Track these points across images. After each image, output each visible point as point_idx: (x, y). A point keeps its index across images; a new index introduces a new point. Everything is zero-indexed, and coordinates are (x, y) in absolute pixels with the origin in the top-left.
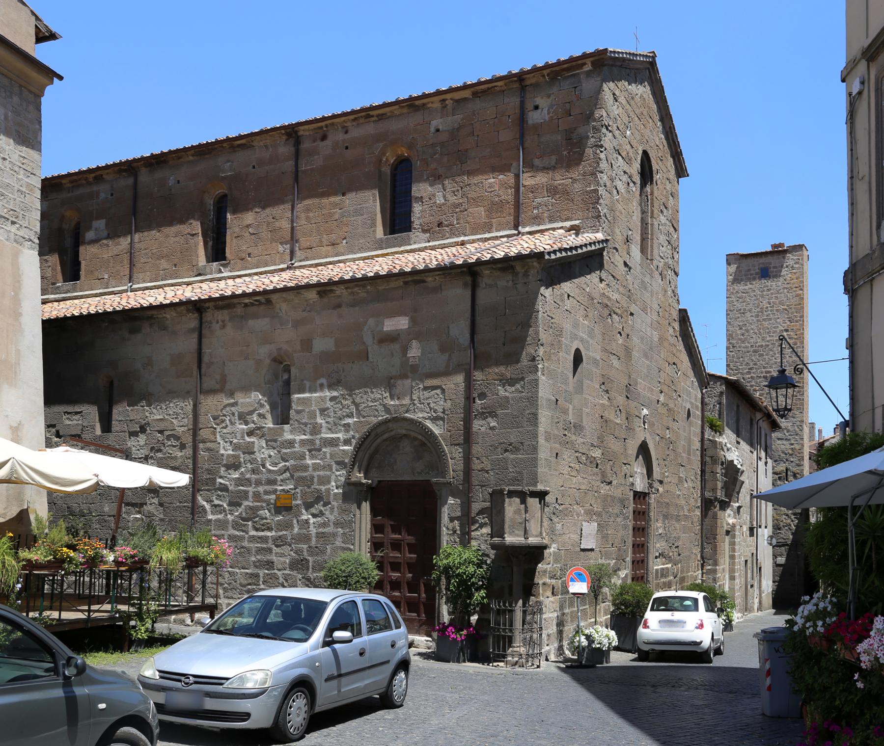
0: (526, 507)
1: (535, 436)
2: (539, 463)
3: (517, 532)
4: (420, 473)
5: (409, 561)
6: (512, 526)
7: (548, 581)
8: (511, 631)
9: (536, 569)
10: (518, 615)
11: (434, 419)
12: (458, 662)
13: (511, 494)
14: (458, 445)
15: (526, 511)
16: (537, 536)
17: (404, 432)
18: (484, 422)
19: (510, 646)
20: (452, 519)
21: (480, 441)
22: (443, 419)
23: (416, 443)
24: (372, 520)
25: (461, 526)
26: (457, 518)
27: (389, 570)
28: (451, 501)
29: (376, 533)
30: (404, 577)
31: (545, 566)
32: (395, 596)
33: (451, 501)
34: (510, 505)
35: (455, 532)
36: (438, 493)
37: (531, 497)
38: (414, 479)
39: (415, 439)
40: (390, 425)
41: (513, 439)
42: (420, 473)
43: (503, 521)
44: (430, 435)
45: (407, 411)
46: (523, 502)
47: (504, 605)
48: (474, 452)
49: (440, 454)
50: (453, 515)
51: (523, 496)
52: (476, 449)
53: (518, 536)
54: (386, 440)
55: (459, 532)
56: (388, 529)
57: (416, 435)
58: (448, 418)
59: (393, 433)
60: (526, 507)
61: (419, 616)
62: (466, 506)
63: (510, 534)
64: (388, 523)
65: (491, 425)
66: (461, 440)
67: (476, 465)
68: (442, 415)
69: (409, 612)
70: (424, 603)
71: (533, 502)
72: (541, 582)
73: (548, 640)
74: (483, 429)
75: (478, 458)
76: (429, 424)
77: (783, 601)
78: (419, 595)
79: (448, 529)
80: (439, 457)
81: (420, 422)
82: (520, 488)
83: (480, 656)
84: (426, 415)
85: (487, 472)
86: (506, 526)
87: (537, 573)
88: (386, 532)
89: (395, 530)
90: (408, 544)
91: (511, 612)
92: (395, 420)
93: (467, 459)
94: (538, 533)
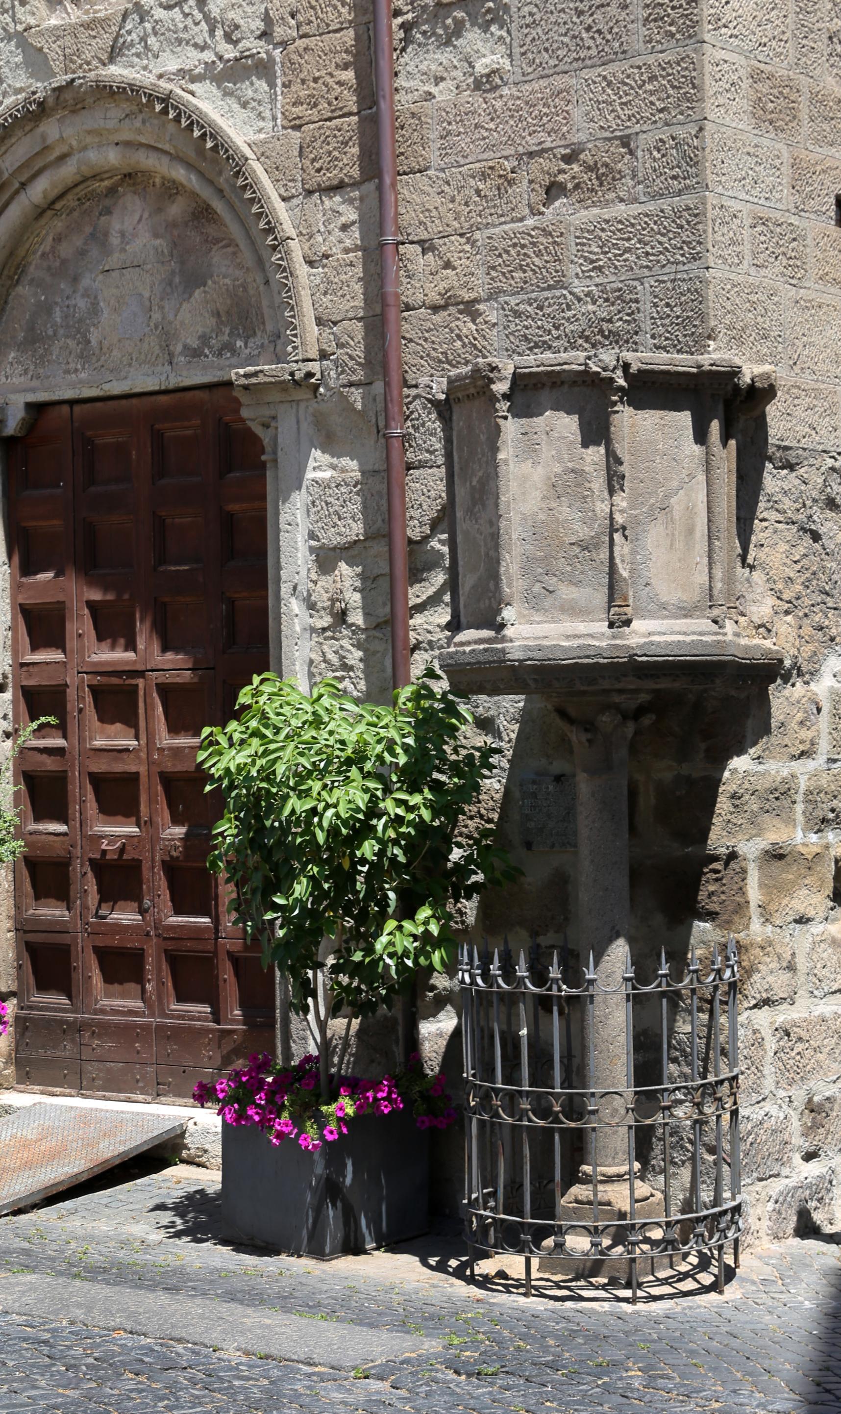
0: (613, 459)
1: (685, 90)
2: (715, 236)
3: (567, 592)
4: (195, 353)
5: (170, 766)
6: (542, 567)
7: (800, 838)
8: (575, 1108)
9: (715, 783)
10: (612, 1023)
11: (231, 74)
12: (318, 1253)
13: (532, 392)
14: (338, 187)
15: (614, 481)
16: (686, 612)
17: (112, 157)
18: (446, 56)
19: (572, 1177)
20: (326, 559)
21: (434, 157)
22: (263, 69)
23: (176, 209)
24: (16, 588)
25: (369, 584)
26: (347, 551)
27: (92, 806)
28: (320, 467)
29: (35, 647)
30: (154, 839)
31: (777, 768)
32: (118, 928)
33: (320, 467)
34: (530, 448)
35: (341, 617)
36: (265, 436)
37: (638, 404)
38: (175, 381)
39: (172, 189)
40: (50, 129)
41: (582, 126)
42: (195, 353)
43: (495, 538)
44: (211, 153)
45: (114, 54)
46: (596, 431)
47: (540, 977)
48: (408, 216)
49: (264, 239)
50: (331, 537)
51: (590, 399)
52: (418, 201)
53: (573, 610)
54: (42, 212)
55: (357, 618)
56: (80, 625)
57: (180, 173)
58: (292, 66)
59: (68, 171)
60: (613, 459)
61: (216, 1017)
62: (381, 492)
63: (533, 602)
64: (78, 595)
65: (481, 67)
66: (348, 163)
67: (419, 279)
68: (259, 48)
69: (180, 999)
70: (234, 959)
71: (657, 435)
72: (750, 849)
73: (808, 1131)
74: (443, 93)
75: (427, 247)
76: (208, 103)
77: (16, 807)
78: (216, 921)
79: (311, 606)
80: (261, 263)
81: (166, 99)
82: (574, 359)
83: (431, 1227)
84: (192, 59)
85: (470, 309)
86: (511, 566)
87: (723, 805)
88: (72, 643)
89: (111, 625)
90: (164, 690)
91: (576, 1008)
92: (68, 100)
93: (377, 255)
94: (695, 591)
